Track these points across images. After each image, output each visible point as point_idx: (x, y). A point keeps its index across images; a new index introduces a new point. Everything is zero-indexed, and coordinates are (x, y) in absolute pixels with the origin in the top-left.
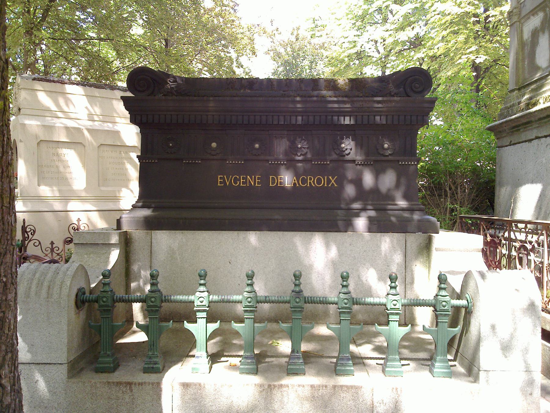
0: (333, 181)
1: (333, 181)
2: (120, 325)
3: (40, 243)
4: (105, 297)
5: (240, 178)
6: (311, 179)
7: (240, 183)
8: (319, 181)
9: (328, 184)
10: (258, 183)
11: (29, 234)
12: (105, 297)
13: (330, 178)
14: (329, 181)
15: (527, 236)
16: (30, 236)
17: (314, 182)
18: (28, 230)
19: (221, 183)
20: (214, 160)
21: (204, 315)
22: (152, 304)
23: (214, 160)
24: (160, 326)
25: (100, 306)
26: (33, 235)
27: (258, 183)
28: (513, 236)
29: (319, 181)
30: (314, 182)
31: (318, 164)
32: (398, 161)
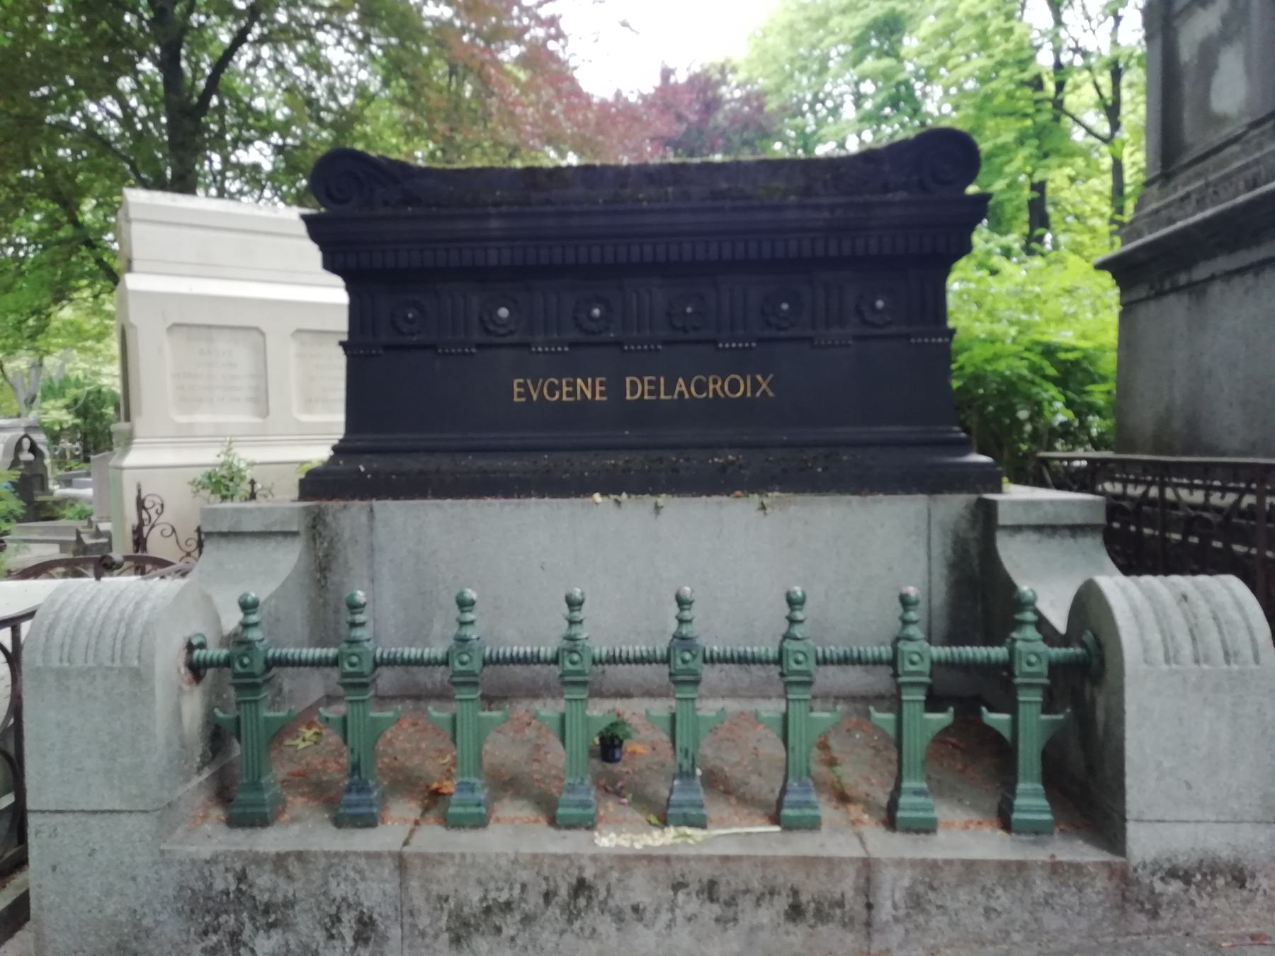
0: (764, 386)
1: (764, 386)
2: (388, 718)
3: (174, 530)
4: (354, 654)
5: (561, 383)
6: (715, 382)
7: (561, 395)
8: (734, 387)
9: (754, 392)
10: (602, 394)
11: (152, 512)
12: (354, 654)
13: (759, 378)
14: (756, 385)
15: (1207, 496)
16: (154, 516)
17: (722, 388)
18: (147, 504)
19: (520, 395)
20: (501, 346)
21: (1037, 697)
22: (912, 668)
23: (501, 346)
24: (480, 719)
25: (236, 675)
26: (159, 514)
27: (602, 394)
28: (1169, 494)
29: (734, 387)
30: (722, 388)
31: (737, 348)
32: (908, 336)
